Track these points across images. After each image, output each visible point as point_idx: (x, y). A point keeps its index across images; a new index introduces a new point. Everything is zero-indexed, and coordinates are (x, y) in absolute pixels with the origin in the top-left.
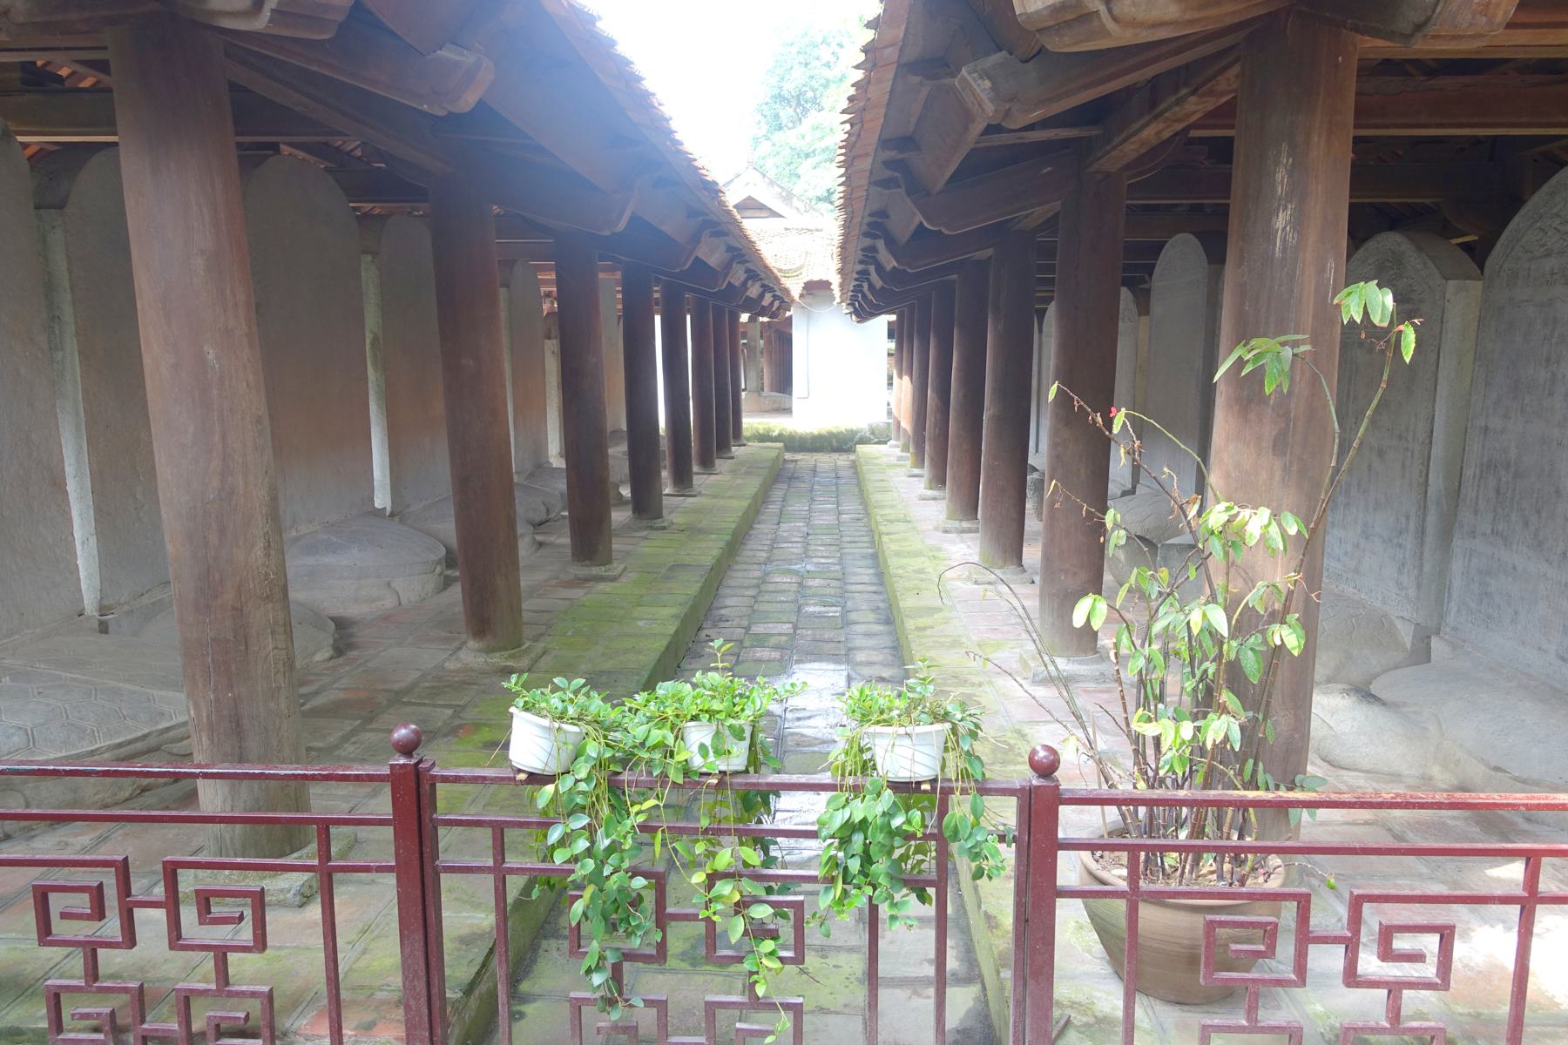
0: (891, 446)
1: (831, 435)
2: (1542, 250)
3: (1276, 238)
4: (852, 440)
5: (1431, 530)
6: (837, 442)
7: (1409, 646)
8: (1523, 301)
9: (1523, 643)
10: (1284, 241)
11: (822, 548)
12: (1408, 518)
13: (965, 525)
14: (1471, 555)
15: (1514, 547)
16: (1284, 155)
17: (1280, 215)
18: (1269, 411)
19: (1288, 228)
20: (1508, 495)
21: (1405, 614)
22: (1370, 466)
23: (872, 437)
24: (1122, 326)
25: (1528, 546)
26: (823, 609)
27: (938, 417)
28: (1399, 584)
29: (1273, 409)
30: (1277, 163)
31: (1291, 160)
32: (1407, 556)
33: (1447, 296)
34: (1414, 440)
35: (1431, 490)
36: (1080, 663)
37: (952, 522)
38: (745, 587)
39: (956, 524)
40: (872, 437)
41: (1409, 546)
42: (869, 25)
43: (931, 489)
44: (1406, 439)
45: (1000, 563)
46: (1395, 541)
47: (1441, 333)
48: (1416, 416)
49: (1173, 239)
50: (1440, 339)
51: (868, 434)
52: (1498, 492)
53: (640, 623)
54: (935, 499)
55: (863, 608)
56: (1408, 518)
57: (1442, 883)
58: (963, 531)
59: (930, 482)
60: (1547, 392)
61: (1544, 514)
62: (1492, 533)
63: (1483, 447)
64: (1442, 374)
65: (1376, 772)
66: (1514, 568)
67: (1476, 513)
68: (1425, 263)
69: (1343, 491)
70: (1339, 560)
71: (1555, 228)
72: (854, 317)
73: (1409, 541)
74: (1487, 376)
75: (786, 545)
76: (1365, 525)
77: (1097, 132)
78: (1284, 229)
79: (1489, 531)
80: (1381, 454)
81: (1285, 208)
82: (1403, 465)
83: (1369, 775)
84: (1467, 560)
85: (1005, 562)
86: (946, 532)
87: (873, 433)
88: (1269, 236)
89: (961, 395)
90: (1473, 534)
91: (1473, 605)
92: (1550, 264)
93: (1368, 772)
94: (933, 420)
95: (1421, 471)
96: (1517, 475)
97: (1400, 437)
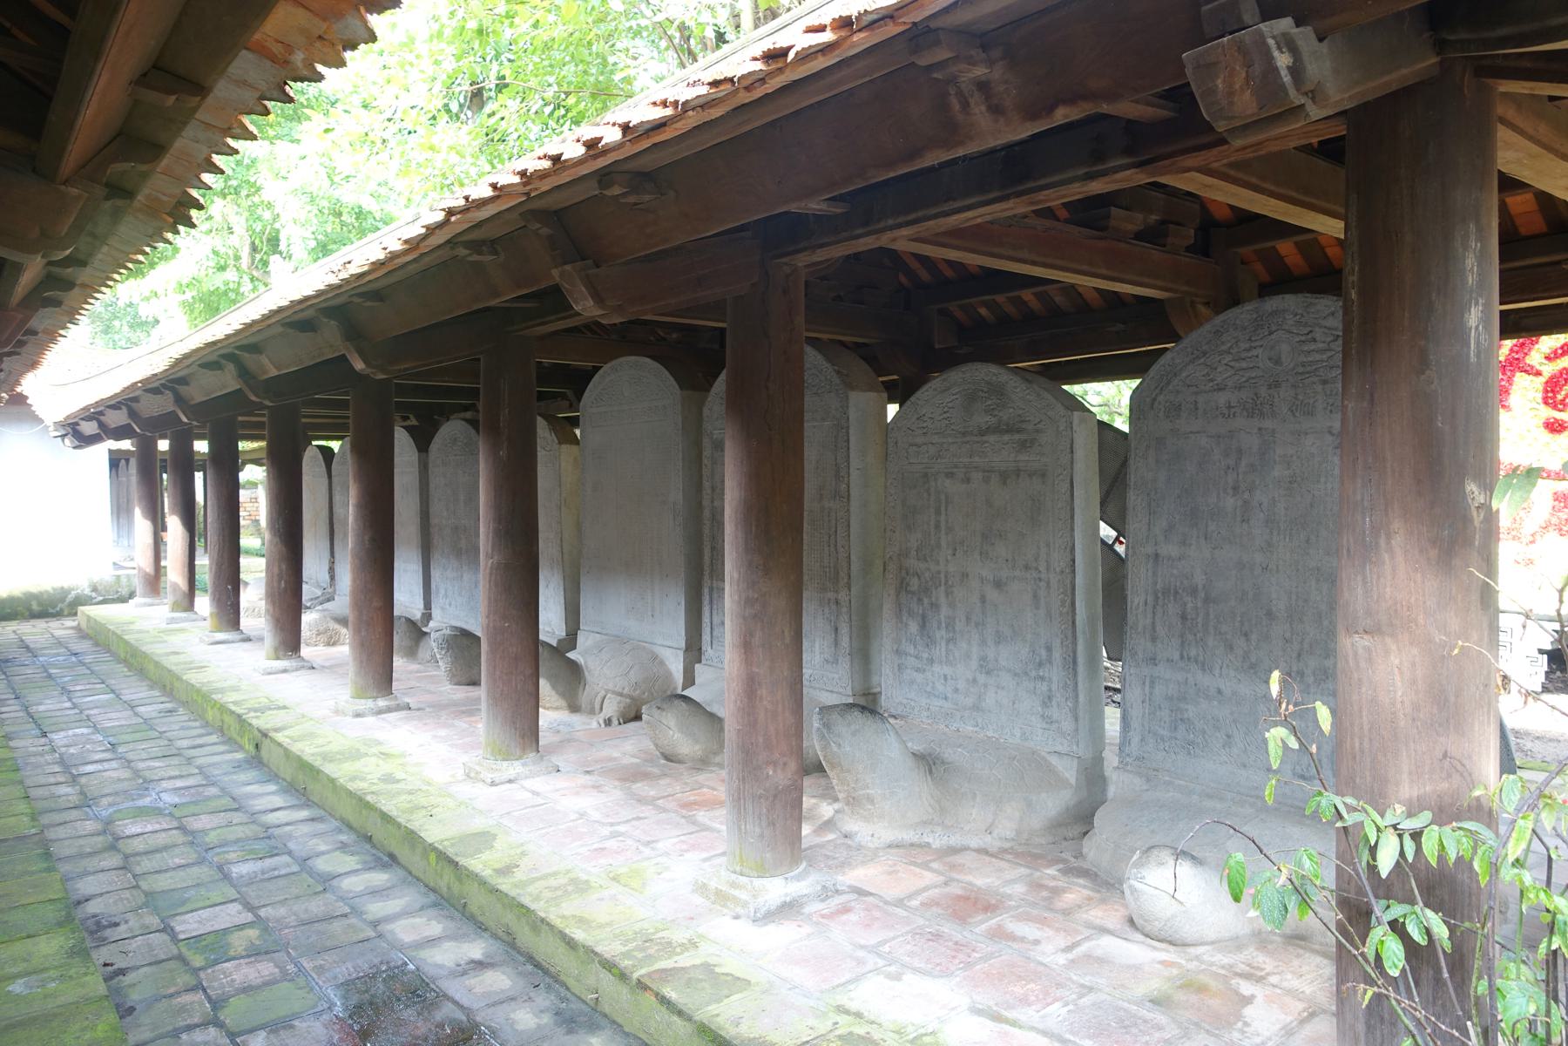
0: (138, 606)
1: (30, 597)
2: (1211, 384)
3: (1469, 337)
4: (63, 600)
5: (1081, 659)
6: (40, 604)
7: (1073, 781)
8: (1191, 432)
9: (1245, 766)
10: (1478, 343)
11: (157, 764)
12: (1049, 649)
13: (382, 703)
14: (1152, 682)
15: (1217, 672)
16: (1473, 237)
17: (1472, 309)
18: (1476, 554)
19: (1481, 328)
20: (1200, 620)
21: (1059, 748)
22: (983, 600)
23: (94, 595)
24: (541, 454)
25: (1236, 670)
26: (259, 865)
27: (284, 567)
28: (1049, 720)
29: (1478, 552)
30: (1466, 248)
31: (1479, 245)
32: (1054, 687)
33: (1074, 428)
34: (1048, 569)
35: (1078, 618)
36: (798, 878)
37: (363, 701)
38: (91, 854)
39: (370, 704)
40: (94, 595)
41: (1055, 679)
42: (372, 37)
43: (278, 658)
44: (1036, 569)
45: (518, 752)
46: (1033, 674)
47: (1072, 463)
48: (1048, 545)
49: (609, 365)
50: (1072, 469)
51: (87, 591)
52: (1184, 617)
53: (17, 987)
54: (285, 671)
55: (323, 848)
56: (1049, 649)
57: (596, 954)
58: (380, 712)
59: (276, 650)
60: (1239, 519)
61: (1254, 637)
62: (1182, 657)
63: (1155, 574)
64: (1077, 502)
65: (1220, 941)
66: (1219, 692)
67: (1154, 639)
68: (1039, 395)
69: (944, 625)
70: (946, 698)
71: (1226, 365)
72: (67, 441)
73: (1056, 673)
74: (1149, 505)
75: (90, 768)
76: (983, 659)
77: (839, 211)
78: (1477, 328)
79: (1176, 656)
80: (998, 584)
81: (1477, 304)
82: (1035, 596)
83: (1216, 945)
84: (1147, 688)
85: (524, 750)
86: (358, 715)
87: (95, 589)
88: (1461, 334)
89: (367, 538)
90: (1153, 660)
91: (1165, 733)
92: (1222, 398)
93: (1212, 943)
94: (736, 575)
95: (1063, 602)
96: (1207, 600)
97: (1027, 568)
